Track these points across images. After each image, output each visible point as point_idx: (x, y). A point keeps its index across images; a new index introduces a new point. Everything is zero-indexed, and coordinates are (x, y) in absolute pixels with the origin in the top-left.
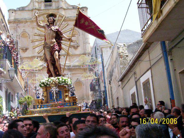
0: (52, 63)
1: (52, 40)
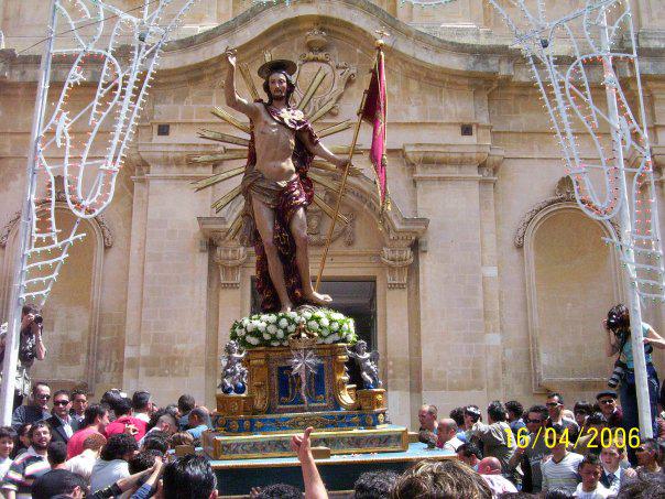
0: (280, 254)
1: (284, 164)
